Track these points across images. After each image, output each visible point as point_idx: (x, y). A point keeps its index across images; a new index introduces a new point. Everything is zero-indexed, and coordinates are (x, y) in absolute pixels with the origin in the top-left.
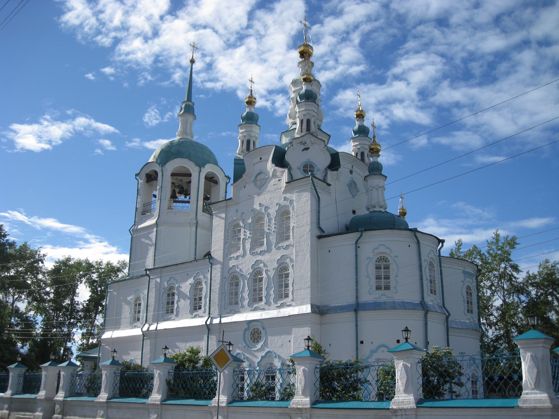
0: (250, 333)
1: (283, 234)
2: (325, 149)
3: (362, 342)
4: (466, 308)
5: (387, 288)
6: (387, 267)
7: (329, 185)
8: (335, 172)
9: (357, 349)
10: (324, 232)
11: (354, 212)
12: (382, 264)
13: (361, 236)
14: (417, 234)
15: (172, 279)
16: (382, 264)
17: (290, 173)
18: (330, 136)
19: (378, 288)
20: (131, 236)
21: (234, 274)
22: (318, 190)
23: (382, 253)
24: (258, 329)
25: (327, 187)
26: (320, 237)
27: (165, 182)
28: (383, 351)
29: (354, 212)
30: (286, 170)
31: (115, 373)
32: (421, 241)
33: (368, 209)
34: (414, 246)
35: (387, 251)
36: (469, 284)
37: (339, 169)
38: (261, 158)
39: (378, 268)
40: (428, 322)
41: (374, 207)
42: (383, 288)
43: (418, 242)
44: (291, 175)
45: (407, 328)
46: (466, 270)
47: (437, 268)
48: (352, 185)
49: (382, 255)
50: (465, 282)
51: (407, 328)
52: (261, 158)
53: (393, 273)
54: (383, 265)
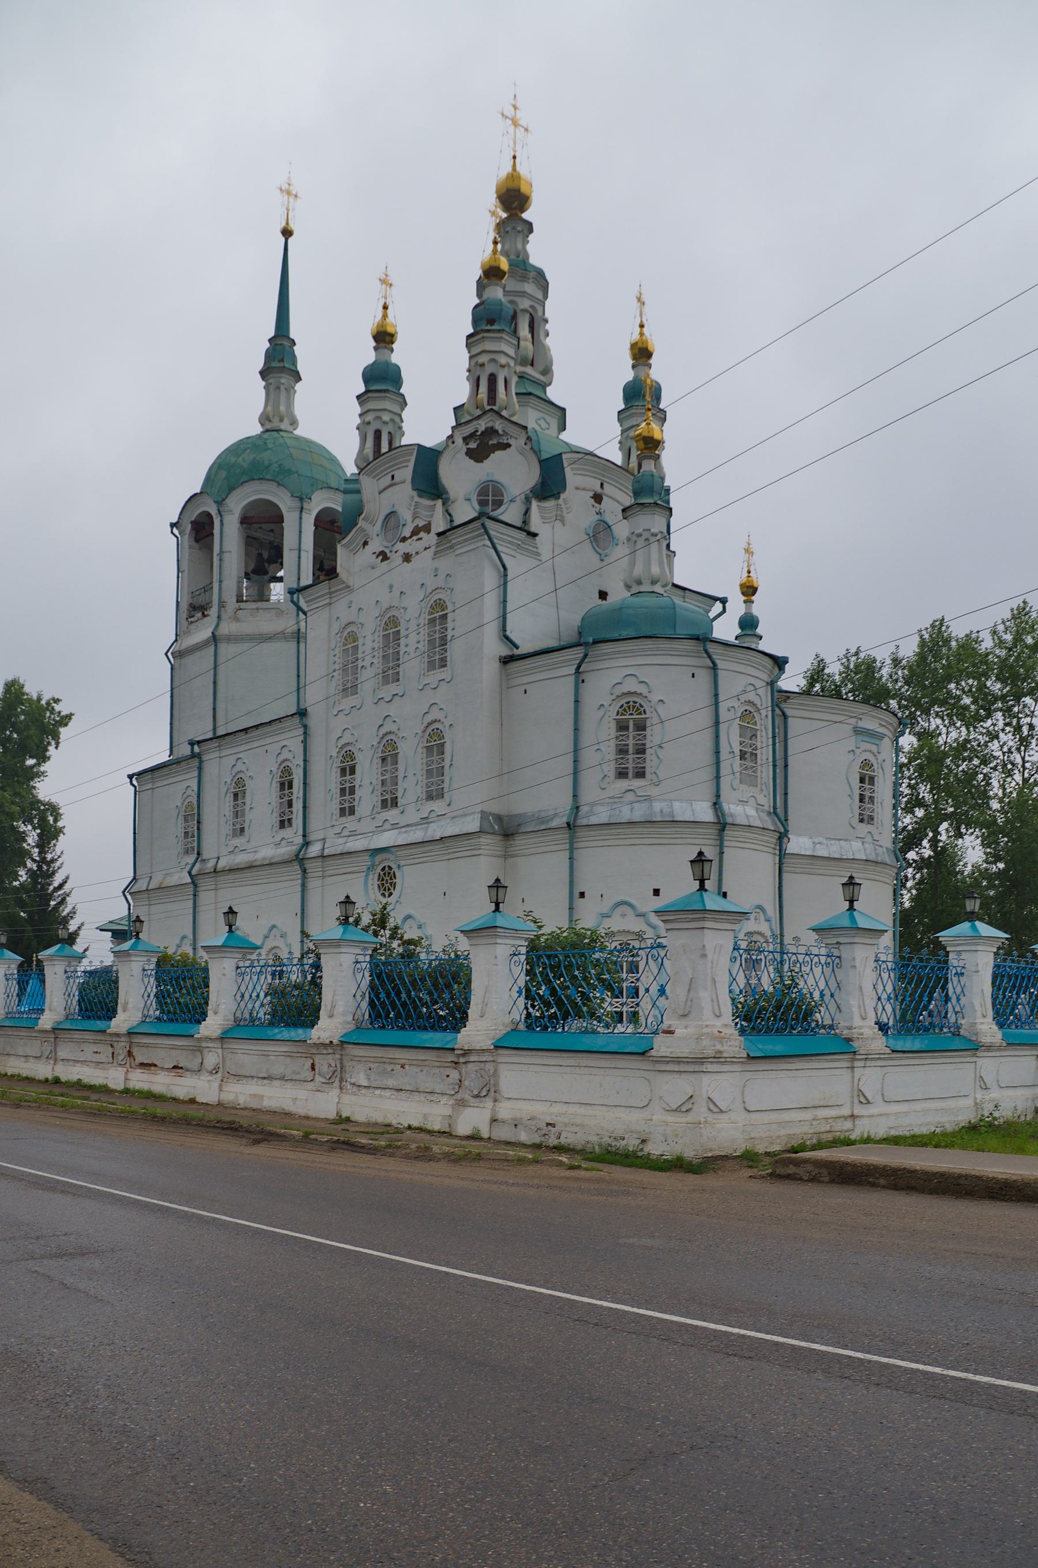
0: (377, 876)
1: (438, 654)
2: (528, 447)
3: (582, 895)
4: (857, 811)
5: (640, 774)
6: (641, 727)
7: (535, 535)
8: (550, 504)
9: (571, 908)
10: (517, 648)
11: (603, 595)
12: (631, 718)
13: (586, 655)
14: (712, 648)
15: (240, 762)
16: (631, 718)
17: (447, 511)
18: (563, 410)
19: (622, 774)
20: (169, 666)
21: (347, 749)
22: (499, 548)
23: (629, 693)
24: (390, 868)
25: (529, 539)
26: (506, 661)
27: (229, 537)
28: (623, 915)
29: (603, 595)
30: (439, 502)
31: (66, 972)
32: (720, 664)
33: (628, 587)
34: (704, 677)
35: (641, 689)
36: (869, 756)
37: (562, 496)
38: (393, 477)
39: (622, 727)
40: (725, 850)
41: (639, 583)
42: (630, 775)
43: (714, 667)
44: (450, 515)
45: (347, 897)
46: (861, 724)
47: (764, 723)
48: (600, 535)
49: (631, 699)
50: (857, 751)
51: (347, 897)
52: (393, 477)
53: (653, 736)
54: (633, 721)
